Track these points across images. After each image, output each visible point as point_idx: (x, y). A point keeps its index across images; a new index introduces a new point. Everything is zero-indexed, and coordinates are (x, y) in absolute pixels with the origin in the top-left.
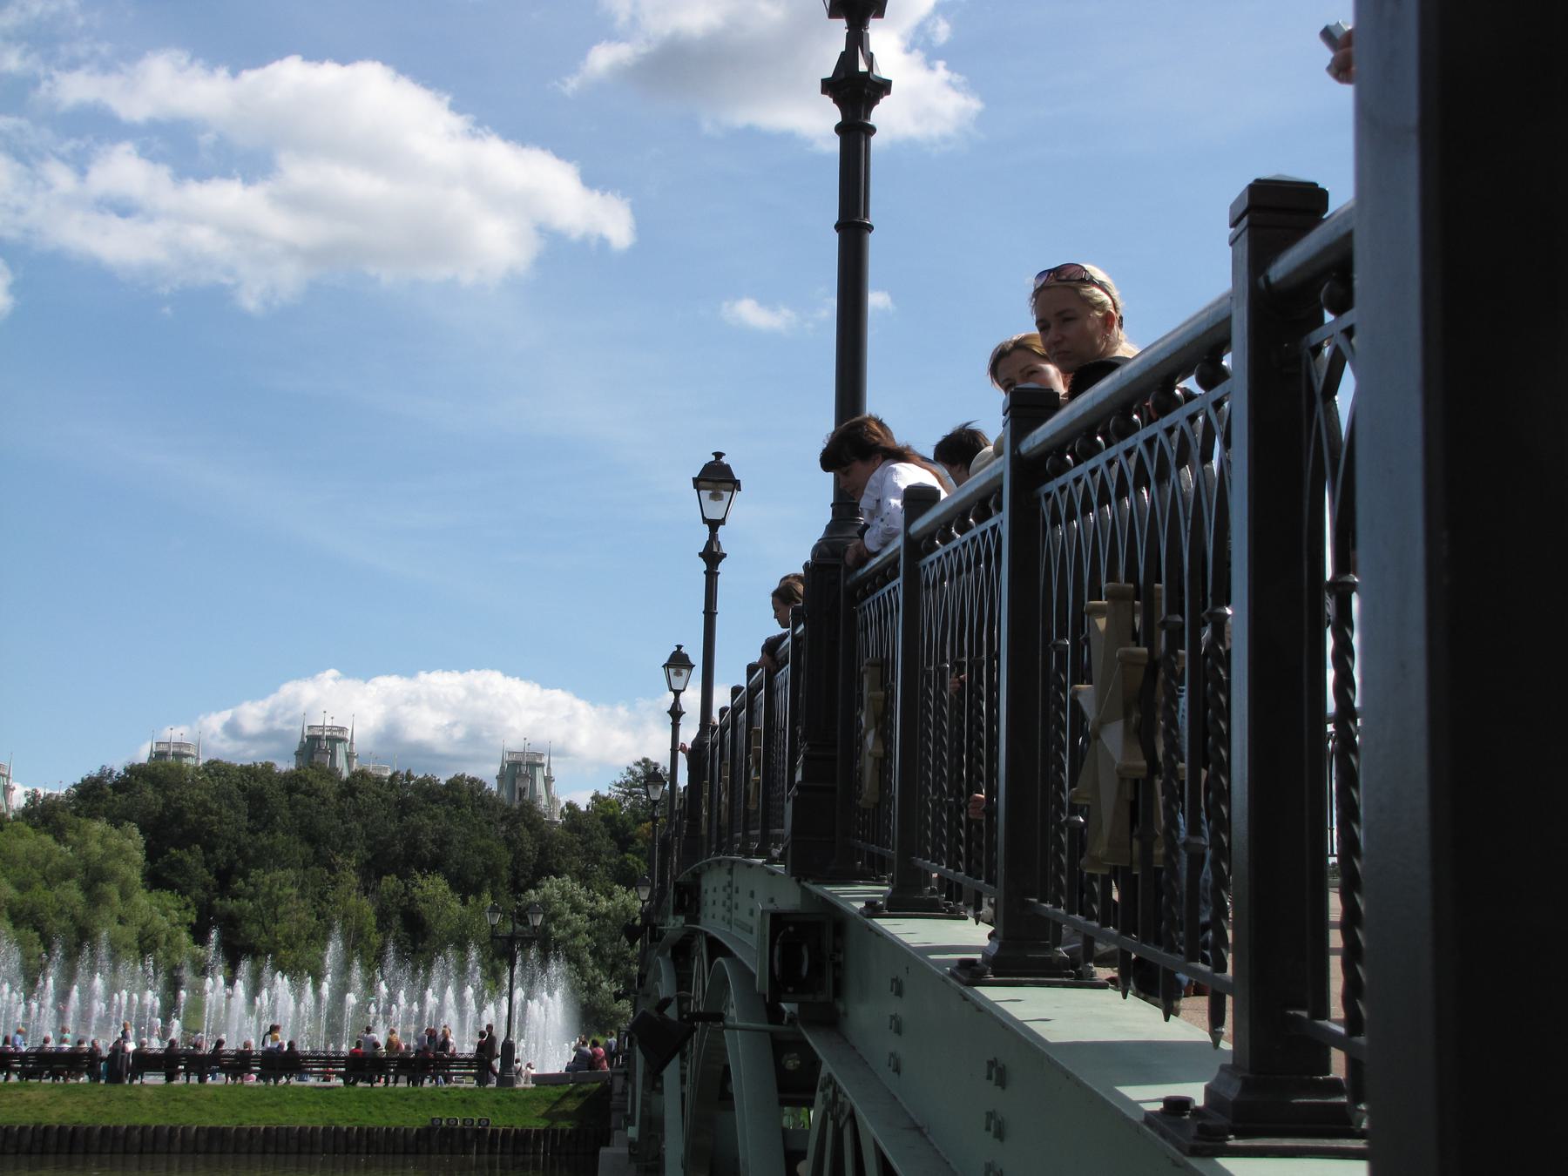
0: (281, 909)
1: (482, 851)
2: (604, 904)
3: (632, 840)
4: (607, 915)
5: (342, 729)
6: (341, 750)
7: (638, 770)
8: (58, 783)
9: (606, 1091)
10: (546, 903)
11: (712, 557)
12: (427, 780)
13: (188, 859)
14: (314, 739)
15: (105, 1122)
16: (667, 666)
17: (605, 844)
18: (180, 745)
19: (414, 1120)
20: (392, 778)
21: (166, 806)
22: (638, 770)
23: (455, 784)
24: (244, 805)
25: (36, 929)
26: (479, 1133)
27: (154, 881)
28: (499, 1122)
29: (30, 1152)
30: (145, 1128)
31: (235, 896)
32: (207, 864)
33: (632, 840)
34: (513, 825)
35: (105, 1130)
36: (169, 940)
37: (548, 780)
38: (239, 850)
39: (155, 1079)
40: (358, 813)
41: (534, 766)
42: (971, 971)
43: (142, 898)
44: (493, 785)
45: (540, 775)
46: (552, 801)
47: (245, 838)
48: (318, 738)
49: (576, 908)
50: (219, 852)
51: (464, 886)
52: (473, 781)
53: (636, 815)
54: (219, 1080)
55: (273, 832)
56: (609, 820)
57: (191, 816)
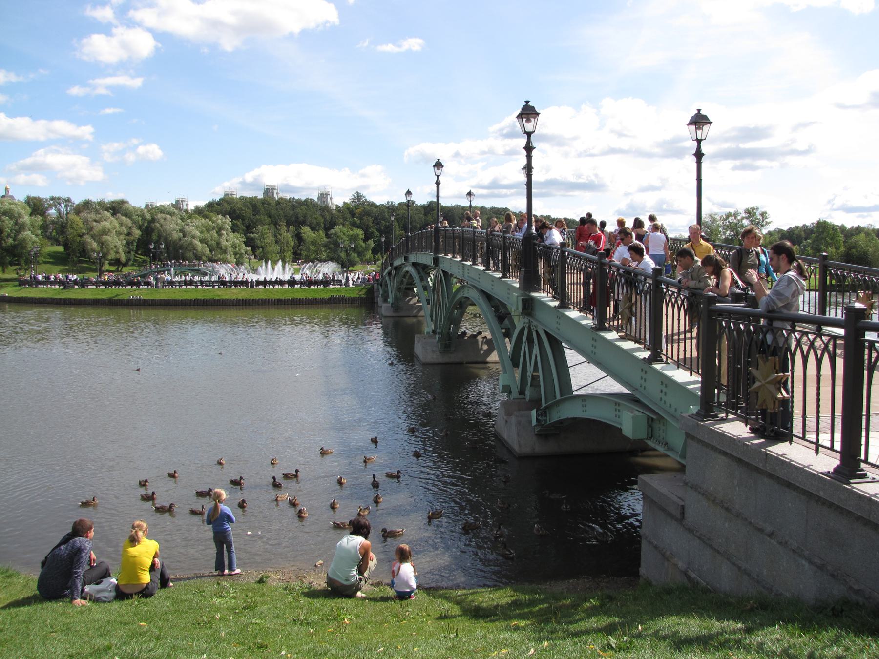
0: (265, 236)
1: (316, 219)
2: (351, 233)
3: (355, 214)
4: (352, 236)
5: (275, 186)
6: (275, 192)
7: (355, 195)
8: (202, 203)
9: (372, 287)
10: (336, 234)
11: (438, 183)
12: (299, 199)
13: (238, 223)
14: (268, 189)
15: (252, 298)
16: (406, 194)
17: (348, 215)
18: (232, 192)
19: (326, 296)
20: (290, 199)
21: (231, 209)
22: (355, 195)
23: (306, 200)
24: (251, 208)
25: (206, 244)
26: (343, 298)
27: (234, 231)
28: (347, 296)
29: (230, 305)
30: (262, 299)
31: (253, 233)
32: (243, 224)
33: (355, 214)
34: (323, 211)
35: (253, 300)
36: (239, 246)
37: (331, 198)
38: (251, 220)
39: (261, 287)
40: (282, 209)
41: (327, 194)
42: (500, 278)
43: (231, 235)
44: (316, 200)
45: (329, 197)
46: (333, 204)
47: (252, 217)
48: (269, 189)
49: (344, 234)
50: (246, 221)
51: (313, 229)
52: (311, 199)
53: (355, 207)
54: (277, 287)
55: (260, 215)
56: (348, 209)
57: (238, 211)
